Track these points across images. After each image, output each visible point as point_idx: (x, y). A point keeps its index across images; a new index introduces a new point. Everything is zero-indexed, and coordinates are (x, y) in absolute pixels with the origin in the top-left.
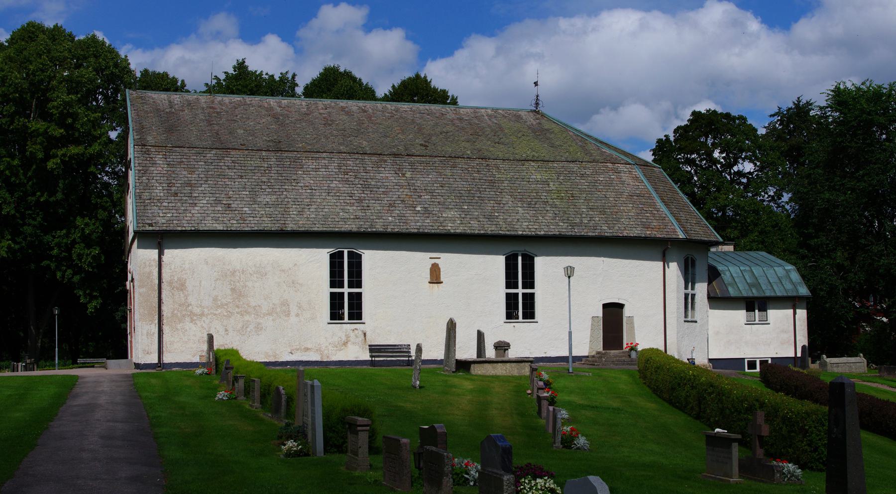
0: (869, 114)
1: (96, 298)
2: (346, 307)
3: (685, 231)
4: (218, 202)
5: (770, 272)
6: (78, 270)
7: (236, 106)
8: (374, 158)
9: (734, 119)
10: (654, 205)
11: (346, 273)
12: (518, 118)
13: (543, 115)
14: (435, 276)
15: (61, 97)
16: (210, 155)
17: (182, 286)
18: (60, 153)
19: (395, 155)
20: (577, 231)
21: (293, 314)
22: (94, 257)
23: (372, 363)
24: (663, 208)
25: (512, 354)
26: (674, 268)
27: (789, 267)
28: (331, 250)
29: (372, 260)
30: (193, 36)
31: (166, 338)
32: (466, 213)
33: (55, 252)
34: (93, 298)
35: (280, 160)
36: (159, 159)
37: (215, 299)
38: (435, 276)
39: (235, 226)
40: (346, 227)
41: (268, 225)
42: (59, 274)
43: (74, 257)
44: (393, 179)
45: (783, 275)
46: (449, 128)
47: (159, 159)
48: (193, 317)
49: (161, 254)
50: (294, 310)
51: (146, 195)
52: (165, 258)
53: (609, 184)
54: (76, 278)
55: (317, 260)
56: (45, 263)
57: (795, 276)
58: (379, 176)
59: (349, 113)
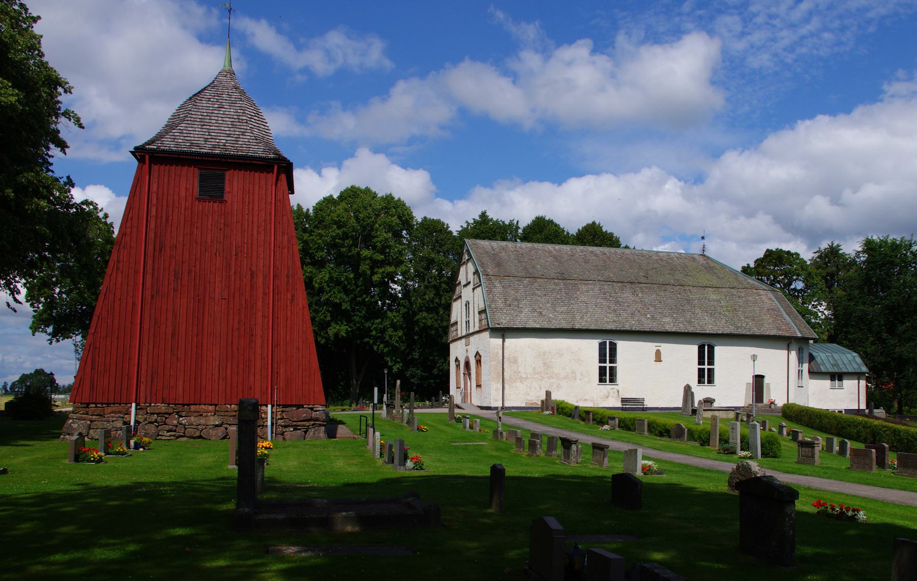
0: (890, 257)
1: (399, 362)
2: (607, 375)
3: (801, 332)
4: (534, 310)
5: (844, 357)
6: (387, 344)
7: (531, 250)
8: (619, 285)
9: (792, 255)
10: (782, 316)
11: (608, 354)
12: (694, 259)
13: (708, 258)
14: (658, 357)
15: (383, 235)
16: (526, 281)
17: (515, 361)
18: (381, 271)
19: (631, 283)
20: (740, 331)
21: (578, 378)
22: (399, 337)
23: (622, 409)
24: (787, 318)
25: (715, 405)
26: (793, 354)
27: (855, 354)
28: (600, 341)
29: (624, 347)
30: (433, 188)
31: (506, 392)
32: (676, 319)
33: (374, 333)
34: (396, 362)
35: (565, 285)
36: (497, 284)
37: (534, 369)
38: (658, 357)
39: (546, 325)
40: (609, 327)
41: (564, 325)
42: (375, 348)
43: (387, 338)
44: (632, 298)
45: (850, 359)
46: (656, 265)
47: (497, 284)
48: (522, 380)
49: (504, 341)
50: (579, 376)
51: (493, 306)
52: (506, 344)
53: (755, 302)
54: (386, 350)
55: (590, 347)
56: (366, 340)
57: (858, 360)
58: (623, 296)
59: (596, 255)
